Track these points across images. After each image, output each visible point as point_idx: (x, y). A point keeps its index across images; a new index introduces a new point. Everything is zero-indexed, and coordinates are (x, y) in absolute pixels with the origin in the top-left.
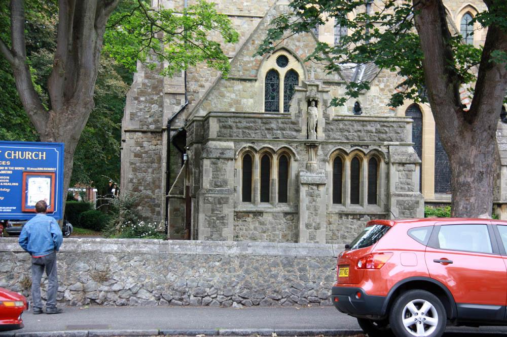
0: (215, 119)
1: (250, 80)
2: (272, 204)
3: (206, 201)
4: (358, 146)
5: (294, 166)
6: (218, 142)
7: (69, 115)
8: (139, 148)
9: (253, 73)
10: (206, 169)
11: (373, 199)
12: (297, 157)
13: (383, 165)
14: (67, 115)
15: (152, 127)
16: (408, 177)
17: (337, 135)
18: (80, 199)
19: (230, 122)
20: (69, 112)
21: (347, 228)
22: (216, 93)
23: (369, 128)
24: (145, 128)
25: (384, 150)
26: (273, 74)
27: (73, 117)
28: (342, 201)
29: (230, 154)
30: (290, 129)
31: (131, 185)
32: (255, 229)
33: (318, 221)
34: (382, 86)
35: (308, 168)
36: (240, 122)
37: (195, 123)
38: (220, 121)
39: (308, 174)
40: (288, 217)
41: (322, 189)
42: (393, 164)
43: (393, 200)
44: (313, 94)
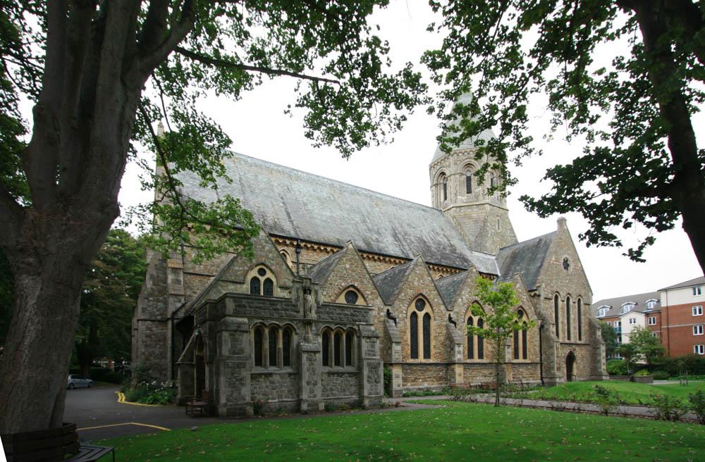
0: (232, 300)
1: (240, 283)
2: (279, 367)
3: (227, 366)
4: (339, 324)
5: (295, 338)
6: (234, 318)
7: (68, 219)
8: (149, 332)
9: (242, 278)
10: (225, 340)
12: (298, 331)
13: (355, 339)
14: (64, 219)
15: (159, 318)
16: (373, 346)
17: (325, 316)
18: (105, 366)
19: (244, 302)
20: (69, 215)
21: (334, 383)
23: (346, 312)
24: (153, 318)
26: (255, 280)
27: (78, 223)
28: (263, 362)
29: (245, 328)
30: (292, 310)
31: (143, 356)
32: (267, 387)
33: (316, 379)
35: (306, 340)
36: (252, 303)
37: (208, 305)
38: (235, 301)
39: (306, 344)
40: (292, 377)
41: (317, 355)
42: (364, 337)
43: (365, 363)
44: (308, 284)
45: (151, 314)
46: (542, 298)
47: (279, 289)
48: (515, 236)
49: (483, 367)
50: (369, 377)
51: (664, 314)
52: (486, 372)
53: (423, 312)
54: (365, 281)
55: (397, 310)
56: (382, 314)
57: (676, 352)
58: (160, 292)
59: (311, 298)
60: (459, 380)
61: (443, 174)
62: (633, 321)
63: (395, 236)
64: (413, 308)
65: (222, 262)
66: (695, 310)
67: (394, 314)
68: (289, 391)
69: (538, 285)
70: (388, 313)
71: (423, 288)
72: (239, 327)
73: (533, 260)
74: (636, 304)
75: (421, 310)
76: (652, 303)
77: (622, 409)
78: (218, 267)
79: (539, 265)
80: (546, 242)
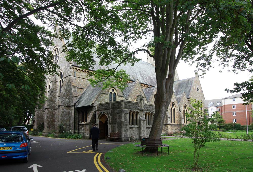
1: (107, 94)
3: (124, 124)
5: (139, 116)
8: (63, 110)
12: (139, 113)
15: (67, 105)
19: (127, 104)
22: (99, 97)
24: (65, 105)
26: (111, 93)
32: (132, 132)
38: (125, 103)
40: (138, 128)
45: (64, 104)
48: (178, 77)
49: (175, 126)
51: (223, 108)
52: (176, 128)
57: (228, 121)
58: (67, 95)
59: (142, 102)
60: (169, 131)
62: (212, 109)
63: (141, 75)
65: (88, 84)
66: (233, 107)
68: (137, 133)
69: (190, 97)
72: (126, 112)
73: (187, 87)
74: (213, 103)
76: (218, 103)
77: (232, 139)
78: (87, 85)
79: (189, 89)
80: (191, 81)
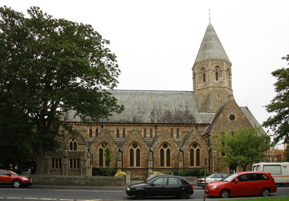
1: (209, 139)
11: (78, 167)
12: (63, 159)
25: (80, 158)
26: (71, 143)
34: (94, 145)
41: (67, 165)
46: (212, 136)
47: (78, 145)
50: (82, 172)
53: (196, 149)
54: (109, 139)
55: (123, 148)
56: (117, 150)
61: (203, 68)
64: (131, 147)
67: (122, 150)
70: (119, 150)
71: (136, 139)
75: (195, 148)
